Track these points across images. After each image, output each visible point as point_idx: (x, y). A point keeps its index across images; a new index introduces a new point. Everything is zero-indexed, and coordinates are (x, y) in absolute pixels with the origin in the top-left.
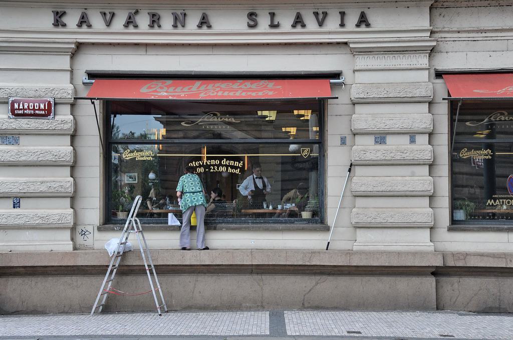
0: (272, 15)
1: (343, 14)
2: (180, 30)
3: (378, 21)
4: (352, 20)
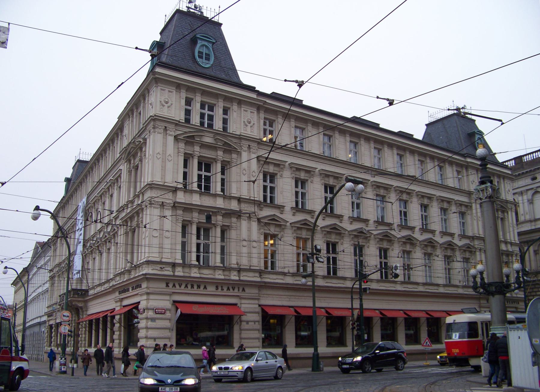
0: (222, 287)
1: (239, 288)
2: (192, 289)
3: (247, 290)
4: (241, 290)
